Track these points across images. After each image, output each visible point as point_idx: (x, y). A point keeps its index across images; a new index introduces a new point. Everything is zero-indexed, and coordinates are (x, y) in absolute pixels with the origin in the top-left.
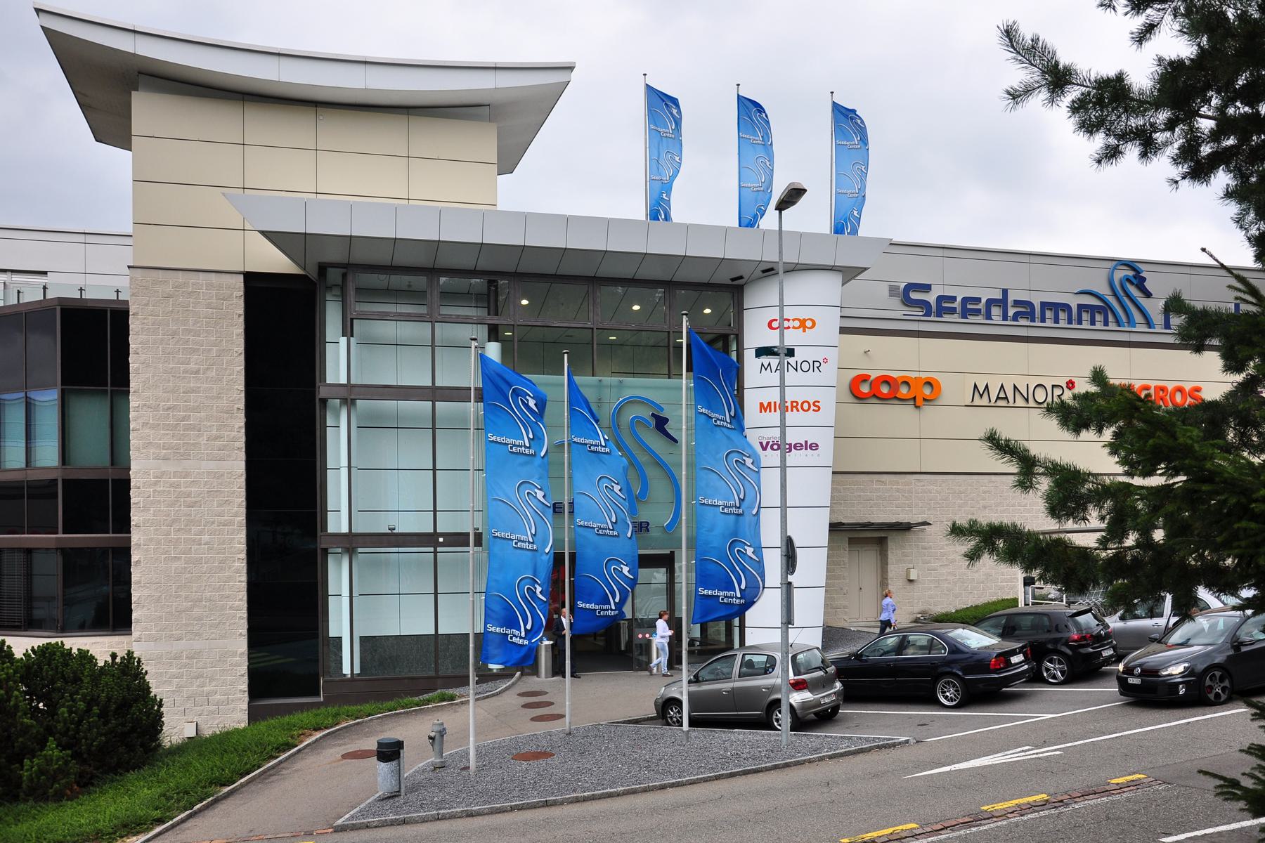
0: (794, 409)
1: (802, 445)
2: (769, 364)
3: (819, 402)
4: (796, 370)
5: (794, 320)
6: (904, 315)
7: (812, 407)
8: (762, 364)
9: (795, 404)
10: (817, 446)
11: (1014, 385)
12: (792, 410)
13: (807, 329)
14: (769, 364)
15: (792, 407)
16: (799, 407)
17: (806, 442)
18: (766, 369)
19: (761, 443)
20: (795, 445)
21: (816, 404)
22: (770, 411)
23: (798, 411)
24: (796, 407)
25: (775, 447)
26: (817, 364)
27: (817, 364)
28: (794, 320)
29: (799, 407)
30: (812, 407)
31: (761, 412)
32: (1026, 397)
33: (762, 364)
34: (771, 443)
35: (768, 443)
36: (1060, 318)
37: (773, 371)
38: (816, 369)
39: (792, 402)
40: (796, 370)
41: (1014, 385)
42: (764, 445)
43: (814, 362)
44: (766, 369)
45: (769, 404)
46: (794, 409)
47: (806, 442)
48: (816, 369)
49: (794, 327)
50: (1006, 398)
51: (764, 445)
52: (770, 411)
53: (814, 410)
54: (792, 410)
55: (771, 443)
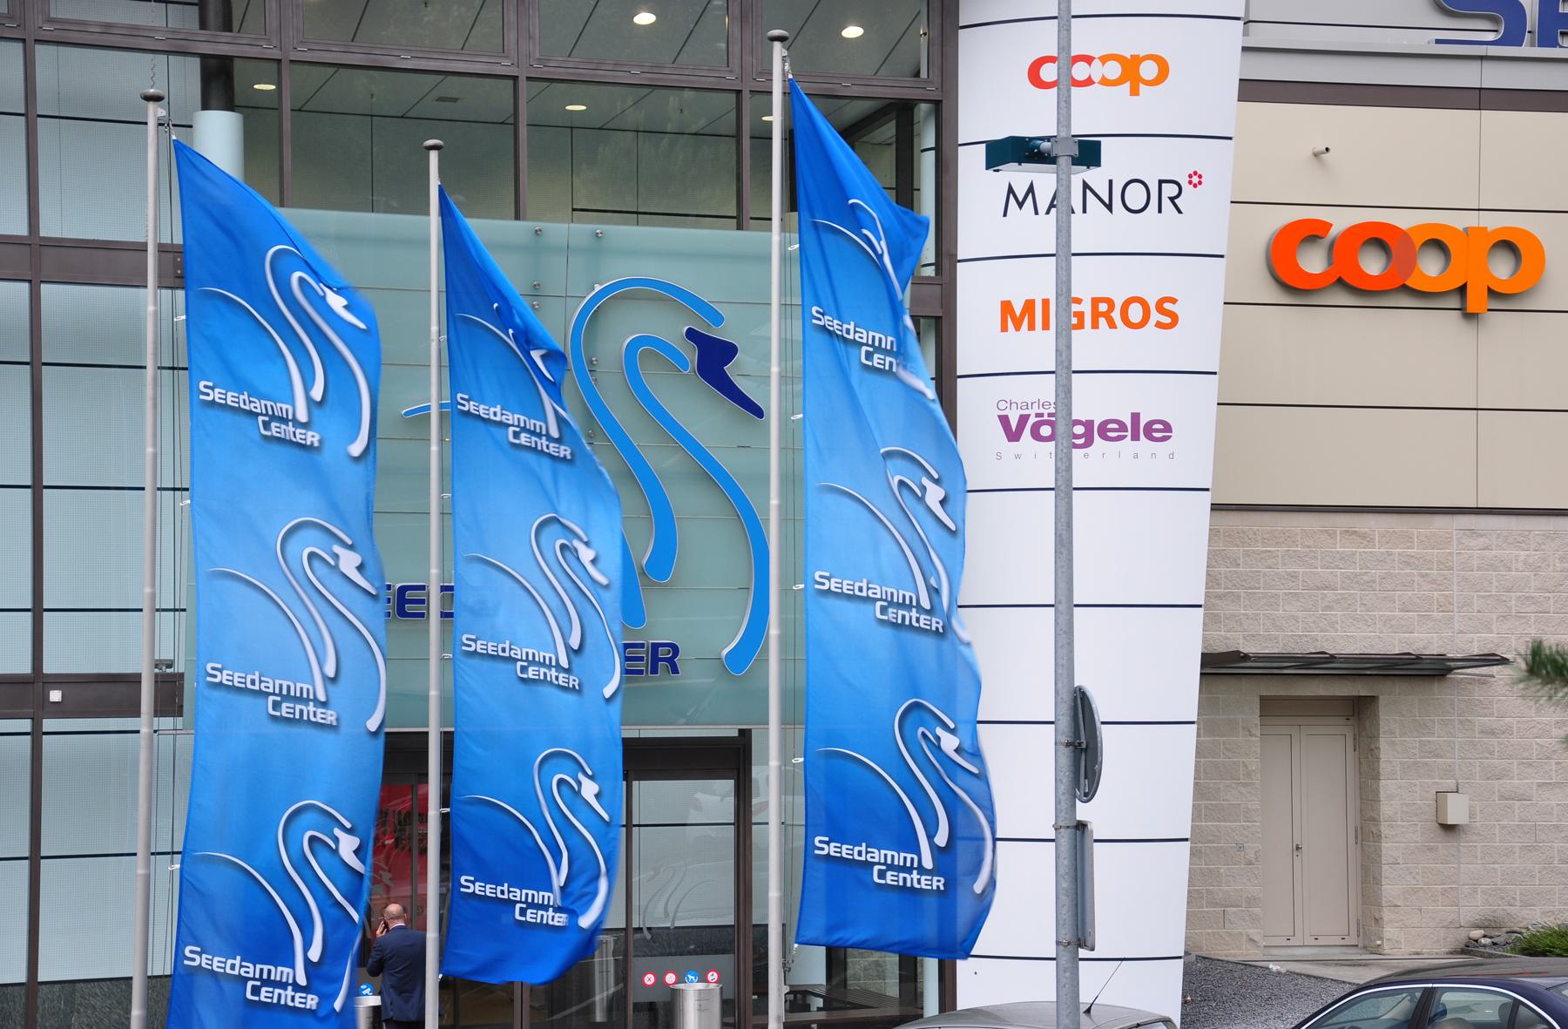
1: (1122, 427)
2: (1031, 190)
3: (1173, 301)
4: (1109, 207)
5: (1105, 59)
7: (1155, 316)
8: (1011, 190)
9: (1103, 307)
10: (1167, 427)
12: (1095, 325)
13: (1142, 86)
14: (1031, 190)
15: (1096, 315)
16: (1116, 315)
18: (1021, 205)
19: (1004, 420)
21: (1167, 306)
22: (1032, 327)
23: (1112, 325)
26: (1170, 190)
27: (1170, 190)
28: (1105, 59)
29: (1116, 315)
30: (1155, 316)
33: (1011, 190)
34: (1032, 420)
35: (1023, 419)
37: (1043, 207)
38: (1166, 203)
39: (1095, 302)
40: (1109, 207)
41: (1031, 185)
43: (1161, 182)
44: (1021, 205)
48: (1166, 203)
49: (1105, 82)
52: (1032, 327)
53: (1159, 325)
54: (1095, 325)
55: (1032, 420)
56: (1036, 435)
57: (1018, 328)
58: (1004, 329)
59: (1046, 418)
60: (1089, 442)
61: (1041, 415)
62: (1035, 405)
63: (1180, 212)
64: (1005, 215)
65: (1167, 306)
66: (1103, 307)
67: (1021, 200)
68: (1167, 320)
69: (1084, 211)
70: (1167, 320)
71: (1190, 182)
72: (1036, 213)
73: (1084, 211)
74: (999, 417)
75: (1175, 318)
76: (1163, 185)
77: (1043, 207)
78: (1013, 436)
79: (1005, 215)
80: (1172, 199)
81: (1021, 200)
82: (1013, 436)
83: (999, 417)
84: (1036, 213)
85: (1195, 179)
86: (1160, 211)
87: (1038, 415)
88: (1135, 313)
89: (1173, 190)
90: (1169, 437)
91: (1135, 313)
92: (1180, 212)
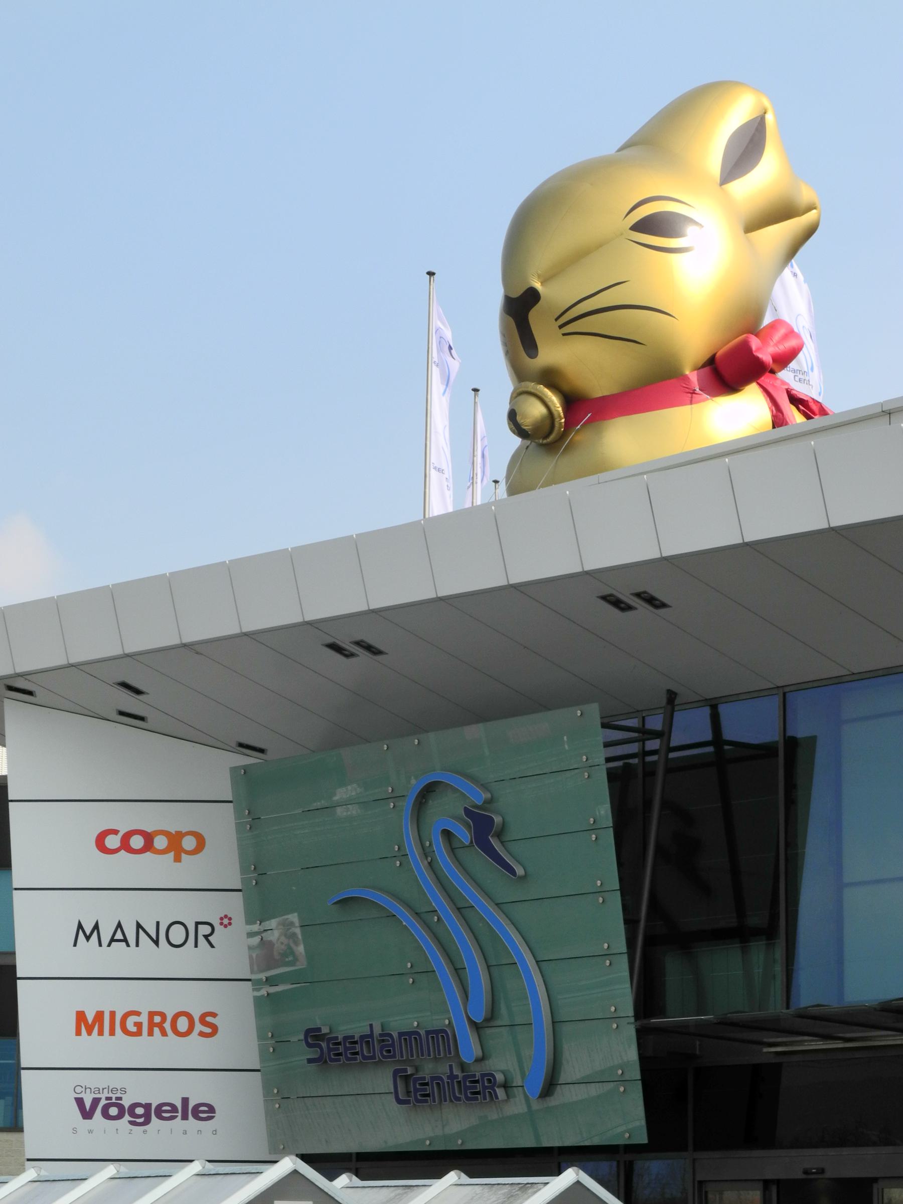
0: (156, 1030)
1: (174, 1108)
2: (96, 927)
3: (214, 1015)
4: (156, 942)
7: (198, 1027)
8: (80, 926)
9: (157, 1019)
10: (211, 1109)
11: (97, 923)
12: (151, 1033)
14: (96, 927)
15: (151, 1025)
16: (167, 1026)
17: (185, 1101)
18: (88, 938)
19: (80, 1102)
20: (160, 1106)
22: (101, 1033)
23: (164, 1033)
25: (113, 1111)
29: (167, 1026)
30: (198, 1027)
33: (80, 926)
35: (96, 1101)
37: (105, 941)
38: (201, 940)
39: (152, 1014)
40: (156, 942)
41: (97, 923)
43: (197, 924)
44: (88, 938)
45: (99, 1016)
46: (156, 1030)
47: (185, 1101)
50: (125, 940)
52: (101, 1033)
53: (202, 1034)
54: (151, 1033)
55: (103, 1102)
56: (106, 1115)
57: (89, 1033)
59: (114, 1101)
60: (147, 1121)
61: (110, 1098)
62: (106, 1091)
64: (75, 945)
67: (88, 934)
70: (208, 1030)
71: (221, 924)
75: (215, 1029)
77: (105, 941)
78: (87, 1114)
81: (88, 934)
82: (87, 1114)
85: (226, 921)
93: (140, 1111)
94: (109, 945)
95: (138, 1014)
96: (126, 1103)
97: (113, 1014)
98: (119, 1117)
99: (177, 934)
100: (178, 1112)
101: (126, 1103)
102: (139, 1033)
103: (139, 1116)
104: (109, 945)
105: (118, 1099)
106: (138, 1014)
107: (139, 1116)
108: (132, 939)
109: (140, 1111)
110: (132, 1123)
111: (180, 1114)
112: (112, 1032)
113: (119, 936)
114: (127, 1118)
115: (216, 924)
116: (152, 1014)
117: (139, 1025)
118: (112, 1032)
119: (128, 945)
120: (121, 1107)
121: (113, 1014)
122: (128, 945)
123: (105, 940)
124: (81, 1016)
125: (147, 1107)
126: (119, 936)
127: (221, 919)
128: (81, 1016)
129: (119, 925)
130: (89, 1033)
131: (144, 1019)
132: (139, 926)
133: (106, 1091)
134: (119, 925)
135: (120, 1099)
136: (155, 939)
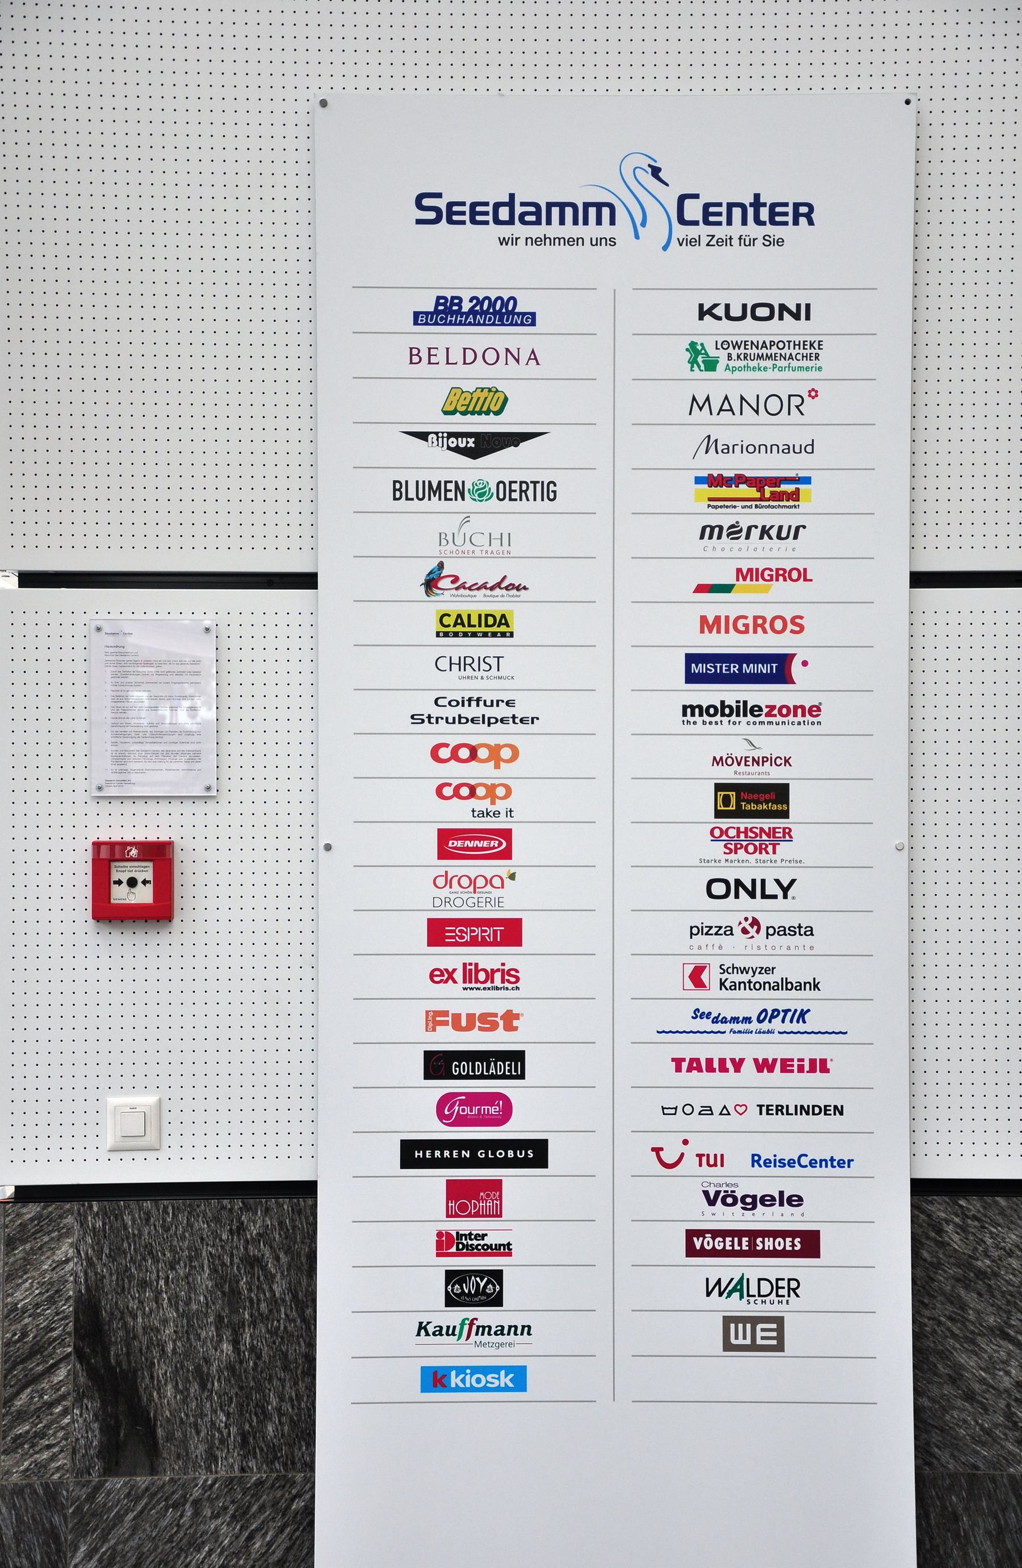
0: (759, 629)
1: (773, 1199)
2: (708, 399)
3: (801, 618)
4: (757, 412)
6: (475, 596)
7: (790, 627)
8: (694, 399)
9: (760, 621)
10: (800, 1199)
11: (708, 397)
12: (755, 632)
14: (708, 399)
15: (756, 626)
16: (767, 626)
17: (781, 1193)
18: (701, 409)
19: (706, 1193)
20: (763, 1198)
21: (798, 621)
22: (719, 632)
23: (765, 631)
24: (762, 626)
25: (729, 1200)
29: (767, 626)
30: (790, 627)
31: (842, 1106)
32: (695, 402)
33: (694, 399)
34: (722, 1194)
35: (718, 1193)
36: (150, 888)
37: (715, 410)
38: (793, 409)
39: (755, 618)
40: (757, 412)
41: (708, 397)
42: (712, 1197)
43: (790, 396)
44: (701, 409)
45: (717, 619)
46: (759, 629)
47: (781, 1193)
50: (731, 410)
51: (712, 1197)
52: (719, 632)
53: (792, 631)
54: (755, 632)
55: (722, 1194)
56: (724, 1203)
57: (710, 632)
58: (702, 631)
59: (729, 1193)
60: (754, 1207)
61: (727, 1191)
62: (724, 1185)
63: (802, 414)
64: (690, 414)
65: (798, 621)
66: (756, 1158)
67: (701, 406)
68: (797, 629)
69: (741, 414)
70: (797, 629)
71: (810, 396)
72: (711, 414)
73: (741, 414)
74: (703, 1191)
75: (802, 628)
76: (792, 397)
77: (715, 410)
78: (712, 1202)
79: (690, 414)
80: (797, 407)
81: (701, 406)
82: (712, 1202)
83: (703, 1191)
84: (711, 414)
85: (813, 394)
86: (789, 414)
87: (725, 1192)
88: (778, 625)
89: (798, 401)
90: (801, 1204)
91: (778, 625)
92: (802, 414)
93: (749, 1200)
94: (718, 414)
95: (746, 617)
96: (739, 1195)
97: (727, 618)
98: (734, 1203)
99: (774, 405)
100: (775, 1201)
101: (739, 1195)
102: (747, 631)
103: (749, 1204)
104: (718, 414)
105: (732, 1192)
106: (746, 617)
107: (749, 1204)
108: (736, 409)
109: (749, 1200)
110: (743, 1208)
111: (777, 1202)
112: (727, 631)
113: (726, 406)
114: (740, 1204)
115: (805, 396)
116: (755, 618)
117: (746, 626)
118: (727, 631)
119: (734, 414)
120: (735, 1198)
121: (727, 618)
122: (734, 414)
123: (715, 409)
124: (704, 619)
125: (754, 1197)
126: (726, 406)
127: (810, 392)
128: (704, 619)
129: (726, 398)
130: (710, 632)
131: (750, 621)
132: (742, 398)
133: (724, 1185)
134: (726, 398)
135: (734, 1192)
136: (750, 889)
